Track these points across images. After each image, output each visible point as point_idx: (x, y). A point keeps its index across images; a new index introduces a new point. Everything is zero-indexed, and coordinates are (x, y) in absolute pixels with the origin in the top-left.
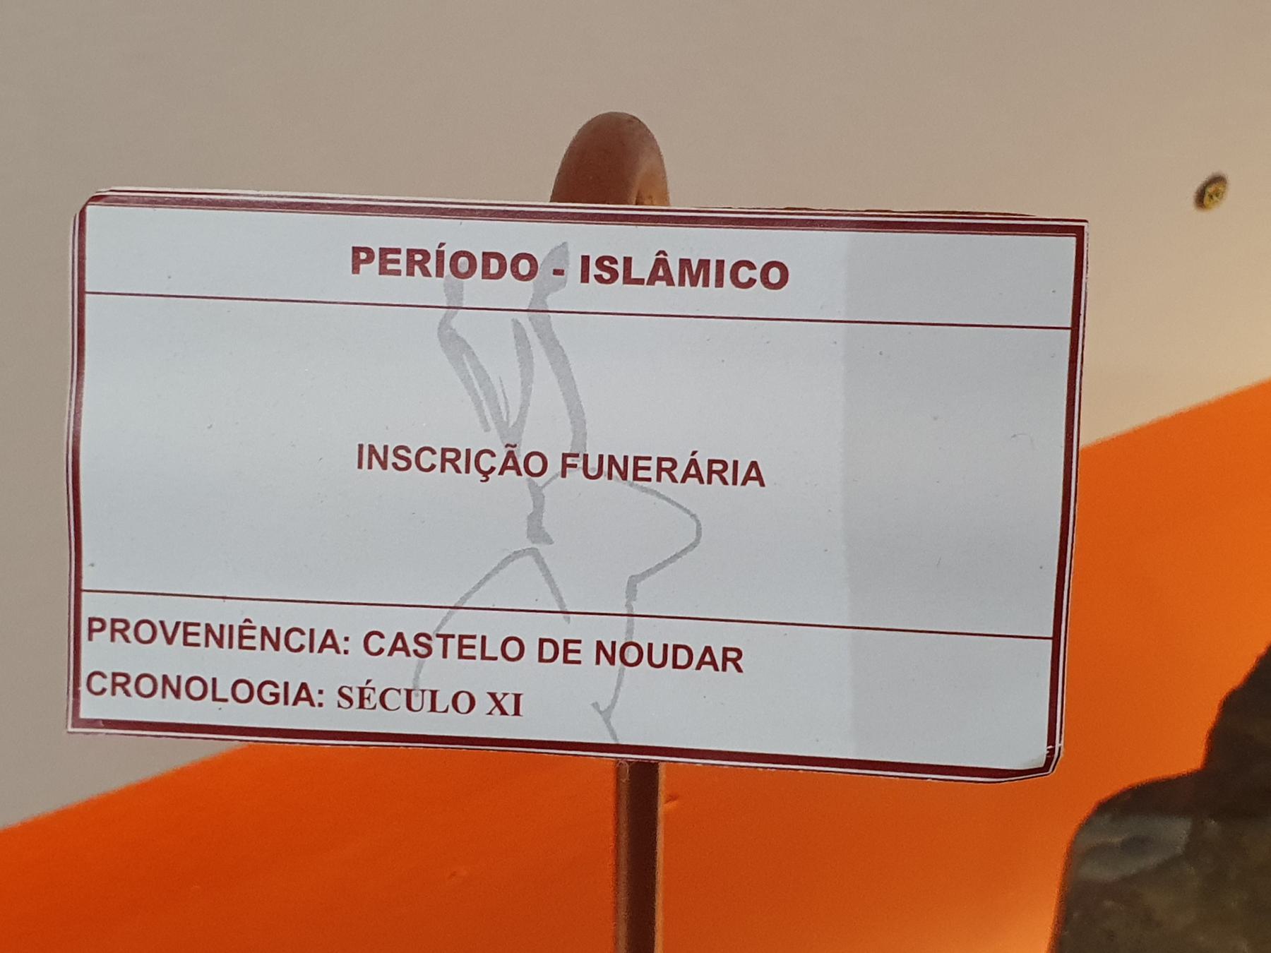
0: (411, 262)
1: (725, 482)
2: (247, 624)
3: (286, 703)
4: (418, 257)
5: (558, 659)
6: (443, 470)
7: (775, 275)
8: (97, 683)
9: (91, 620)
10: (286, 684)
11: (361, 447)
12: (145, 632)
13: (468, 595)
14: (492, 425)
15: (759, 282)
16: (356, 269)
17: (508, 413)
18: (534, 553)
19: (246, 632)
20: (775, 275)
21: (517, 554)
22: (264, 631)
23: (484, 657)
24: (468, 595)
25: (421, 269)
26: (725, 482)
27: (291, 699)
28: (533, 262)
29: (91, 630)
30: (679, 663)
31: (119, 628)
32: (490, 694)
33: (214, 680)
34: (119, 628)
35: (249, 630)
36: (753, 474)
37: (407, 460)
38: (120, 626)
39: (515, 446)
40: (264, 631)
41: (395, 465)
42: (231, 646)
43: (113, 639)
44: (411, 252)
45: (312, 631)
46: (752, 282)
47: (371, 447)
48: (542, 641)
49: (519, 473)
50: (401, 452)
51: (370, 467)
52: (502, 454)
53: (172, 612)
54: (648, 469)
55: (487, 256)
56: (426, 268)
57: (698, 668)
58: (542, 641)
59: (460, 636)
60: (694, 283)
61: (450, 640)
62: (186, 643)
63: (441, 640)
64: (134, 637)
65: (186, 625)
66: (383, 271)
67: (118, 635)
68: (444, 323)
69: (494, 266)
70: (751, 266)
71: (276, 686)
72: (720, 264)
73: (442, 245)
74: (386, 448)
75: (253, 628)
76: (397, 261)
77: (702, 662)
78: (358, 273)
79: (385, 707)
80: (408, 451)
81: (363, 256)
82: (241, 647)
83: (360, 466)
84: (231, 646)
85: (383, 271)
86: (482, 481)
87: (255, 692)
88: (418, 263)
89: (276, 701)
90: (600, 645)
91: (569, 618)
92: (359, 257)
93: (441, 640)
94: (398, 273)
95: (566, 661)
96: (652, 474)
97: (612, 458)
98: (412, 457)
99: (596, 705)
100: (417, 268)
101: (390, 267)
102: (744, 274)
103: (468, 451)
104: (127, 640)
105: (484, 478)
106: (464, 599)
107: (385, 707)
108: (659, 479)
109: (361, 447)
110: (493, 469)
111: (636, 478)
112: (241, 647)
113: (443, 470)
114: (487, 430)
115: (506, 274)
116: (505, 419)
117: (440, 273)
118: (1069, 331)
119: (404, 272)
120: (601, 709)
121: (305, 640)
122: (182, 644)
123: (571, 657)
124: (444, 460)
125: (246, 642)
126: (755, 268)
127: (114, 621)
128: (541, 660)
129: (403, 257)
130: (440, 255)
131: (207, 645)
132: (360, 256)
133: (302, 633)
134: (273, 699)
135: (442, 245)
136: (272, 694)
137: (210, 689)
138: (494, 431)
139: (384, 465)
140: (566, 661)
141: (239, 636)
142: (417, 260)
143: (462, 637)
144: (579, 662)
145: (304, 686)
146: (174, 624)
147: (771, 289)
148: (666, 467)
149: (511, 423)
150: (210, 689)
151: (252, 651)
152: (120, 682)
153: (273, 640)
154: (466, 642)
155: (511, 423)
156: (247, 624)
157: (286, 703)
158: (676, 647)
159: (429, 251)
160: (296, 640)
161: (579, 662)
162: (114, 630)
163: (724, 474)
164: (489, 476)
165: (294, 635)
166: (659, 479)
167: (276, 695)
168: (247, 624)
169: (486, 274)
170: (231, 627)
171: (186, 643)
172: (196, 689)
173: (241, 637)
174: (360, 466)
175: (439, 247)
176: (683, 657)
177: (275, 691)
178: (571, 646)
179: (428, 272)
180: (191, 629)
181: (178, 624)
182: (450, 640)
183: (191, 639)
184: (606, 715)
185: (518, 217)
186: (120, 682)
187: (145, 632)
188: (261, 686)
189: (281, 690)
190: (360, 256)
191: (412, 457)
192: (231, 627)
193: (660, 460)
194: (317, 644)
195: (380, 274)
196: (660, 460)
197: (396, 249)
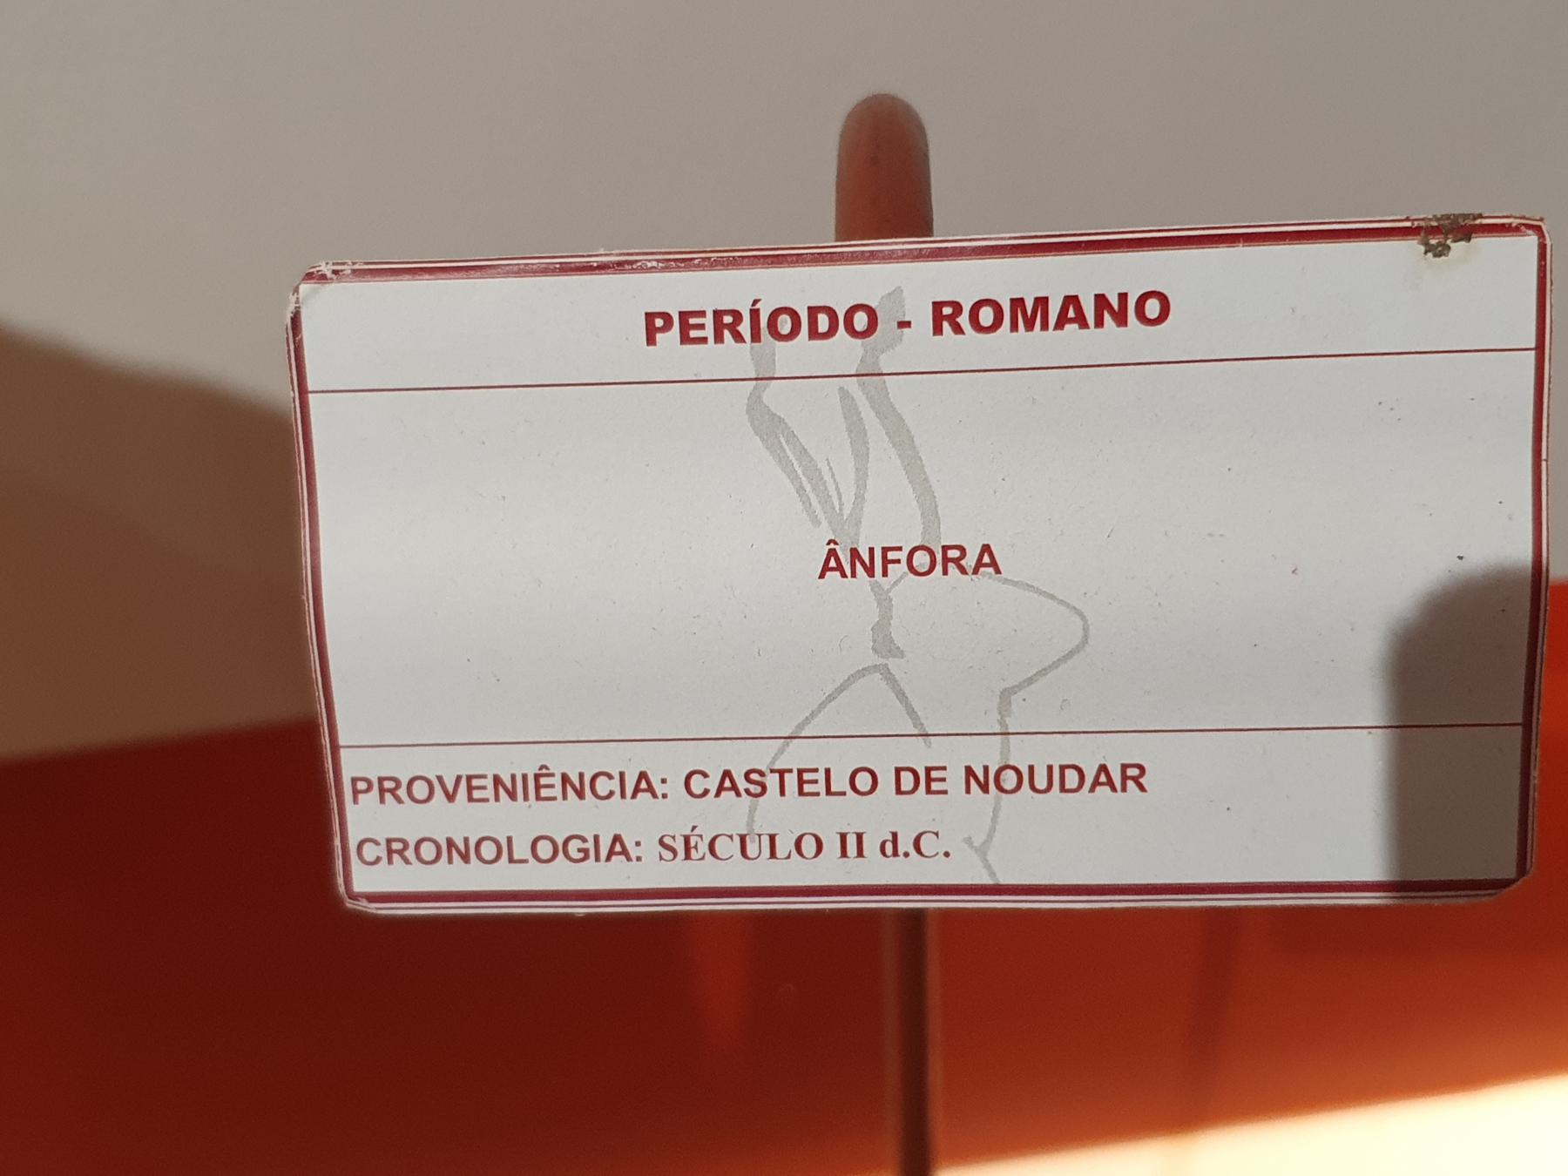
2: (544, 771)
9: (354, 780)
10: (596, 839)
12: (420, 790)
13: (807, 721)
14: (821, 516)
16: (651, 340)
21: (863, 672)
22: (565, 779)
23: (829, 792)
24: (807, 721)
29: (356, 792)
30: (1068, 786)
31: (387, 788)
33: (509, 840)
34: (387, 788)
43: (382, 800)
44: (718, 315)
45: (622, 775)
53: (450, 765)
55: (814, 312)
56: (738, 332)
57: (1092, 790)
58: (898, 771)
60: (1030, 326)
62: (471, 799)
63: (777, 775)
65: (469, 778)
66: (685, 339)
67: (388, 796)
68: (755, 403)
69: (823, 323)
76: (702, 327)
77: (1096, 783)
82: (538, 798)
84: (526, 798)
85: (685, 339)
89: (586, 857)
90: (969, 772)
95: (929, 791)
99: (969, 841)
106: (800, 727)
112: (538, 798)
115: (839, 332)
121: (615, 785)
127: (381, 780)
128: (899, 791)
129: (709, 321)
130: (755, 314)
132: (654, 325)
134: (581, 855)
135: (756, 302)
136: (580, 850)
137: (505, 850)
141: (536, 785)
142: (726, 323)
143: (800, 772)
144: (945, 792)
150: (505, 850)
152: (395, 849)
153: (575, 787)
154: (806, 776)
157: (597, 859)
158: (1063, 768)
161: (945, 792)
162: (382, 791)
169: (814, 334)
170: (525, 777)
172: (488, 850)
173: (538, 787)
176: (1072, 779)
181: (459, 779)
184: (982, 851)
186: (395, 849)
188: (566, 842)
189: (590, 845)
190: (654, 325)
192: (525, 777)
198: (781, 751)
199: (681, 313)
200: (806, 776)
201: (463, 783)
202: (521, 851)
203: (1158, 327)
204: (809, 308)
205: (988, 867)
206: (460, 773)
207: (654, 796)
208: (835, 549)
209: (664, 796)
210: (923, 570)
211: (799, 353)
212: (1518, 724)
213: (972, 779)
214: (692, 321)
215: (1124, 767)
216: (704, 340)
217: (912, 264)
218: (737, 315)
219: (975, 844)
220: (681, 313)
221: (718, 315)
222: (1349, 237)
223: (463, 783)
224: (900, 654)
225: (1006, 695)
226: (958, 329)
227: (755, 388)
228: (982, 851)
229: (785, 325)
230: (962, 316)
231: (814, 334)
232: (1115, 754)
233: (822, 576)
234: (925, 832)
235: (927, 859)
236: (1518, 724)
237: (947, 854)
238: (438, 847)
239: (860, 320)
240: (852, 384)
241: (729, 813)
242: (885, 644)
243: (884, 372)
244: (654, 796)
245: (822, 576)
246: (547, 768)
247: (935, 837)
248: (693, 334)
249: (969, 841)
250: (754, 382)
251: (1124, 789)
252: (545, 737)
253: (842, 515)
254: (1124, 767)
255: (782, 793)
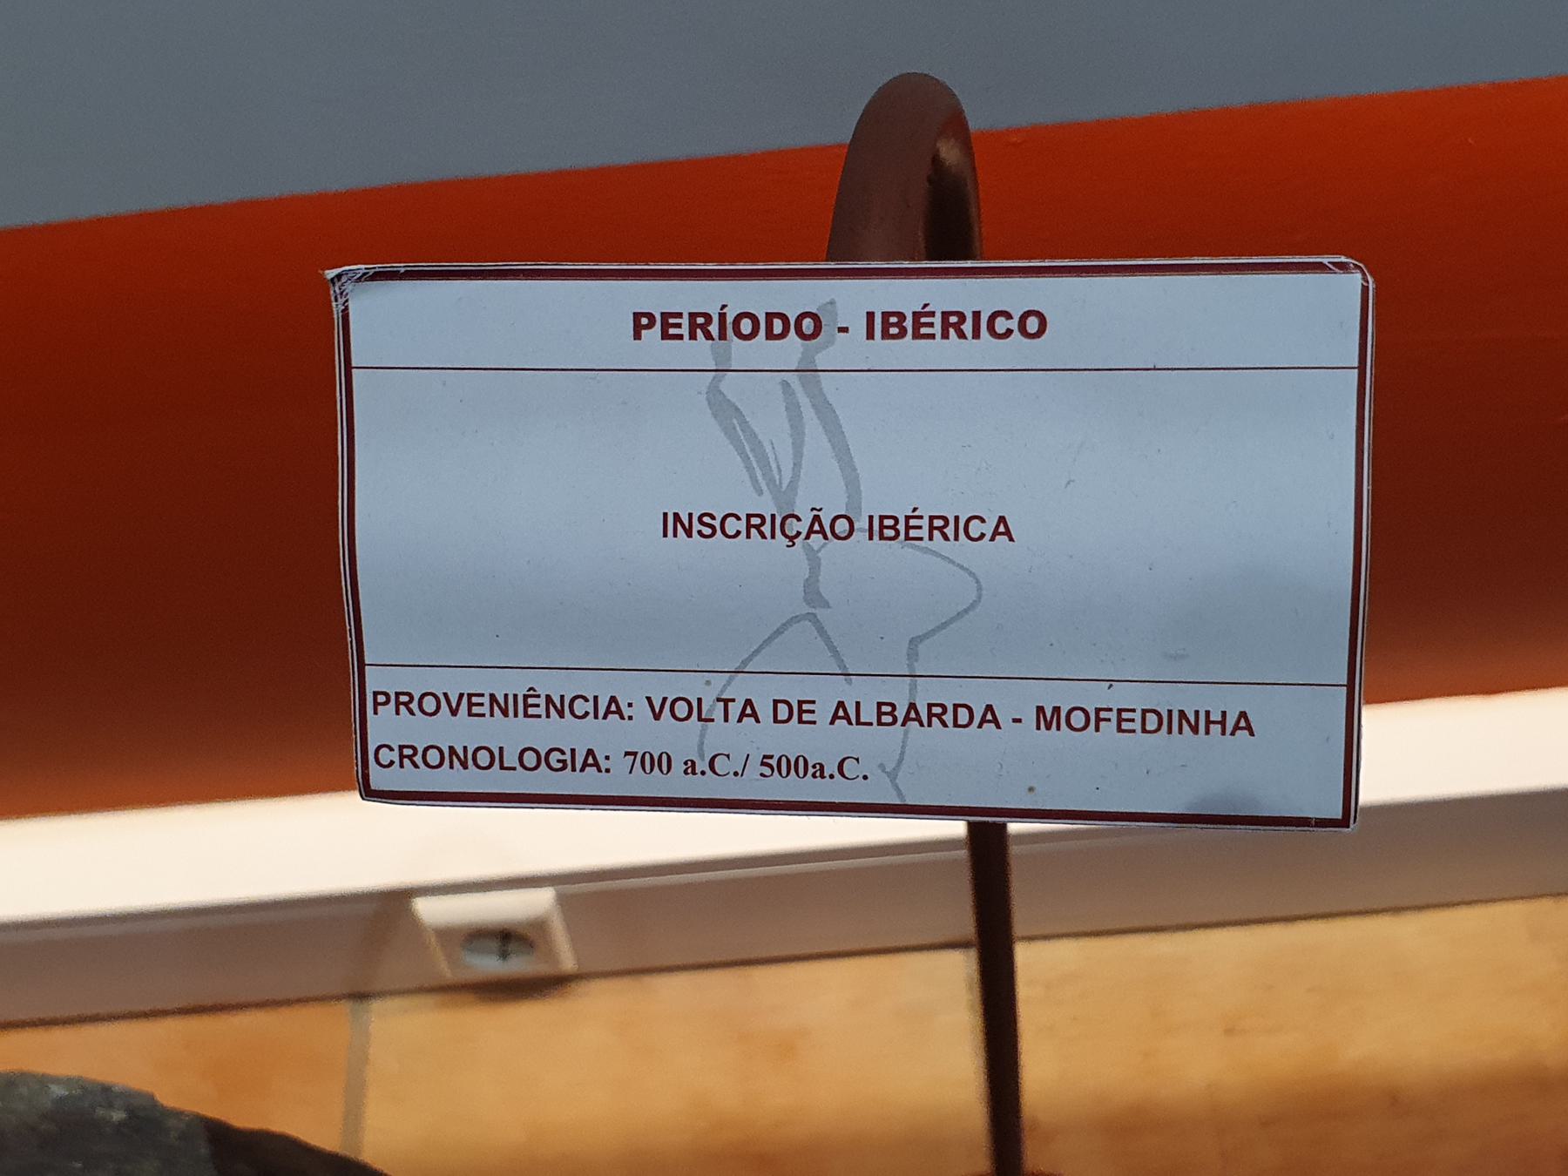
0: (693, 327)
1: (764, 537)
2: (532, 692)
3: (574, 769)
4: (953, 319)
5: (793, 720)
6: (748, 536)
7: (1032, 324)
8: (385, 755)
9: (376, 694)
10: (573, 751)
11: (665, 515)
12: (430, 704)
13: (750, 659)
14: (764, 488)
15: (1016, 333)
16: (637, 336)
17: (781, 476)
18: (812, 618)
19: (531, 701)
20: (1032, 324)
21: (796, 619)
22: (549, 699)
23: (1144, 731)
24: (750, 659)
25: (955, 331)
26: (763, 536)
27: (578, 766)
28: (818, 324)
29: (376, 704)
30: (960, 722)
31: (403, 701)
32: (625, 756)
33: (501, 749)
34: (403, 701)
35: (1126, 713)
36: (1002, 529)
37: (712, 527)
38: (404, 699)
39: (820, 510)
40: (549, 699)
41: (700, 532)
42: (516, 715)
43: (398, 713)
44: (693, 316)
45: (596, 698)
46: (1009, 332)
47: (676, 516)
48: (776, 702)
49: (826, 537)
50: (706, 519)
51: (675, 535)
52: (807, 519)
53: (453, 684)
54: (920, 527)
55: (770, 316)
56: (962, 330)
57: (980, 726)
58: (776, 702)
59: (1118, 709)
61: (730, 704)
62: (470, 714)
63: (722, 704)
64: (418, 710)
65: (470, 696)
66: (665, 336)
67: (402, 708)
68: (714, 390)
69: (778, 326)
70: (1008, 316)
71: (563, 753)
72: (977, 315)
73: (724, 307)
74: (690, 515)
75: (538, 696)
76: (931, 325)
77: (983, 721)
78: (640, 339)
79: (843, 776)
80: (713, 518)
81: (644, 321)
82: (526, 715)
83: (665, 535)
84: (516, 715)
85: (665, 336)
86: (788, 546)
87: (543, 759)
88: (953, 325)
89: (564, 768)
90: (1040, 710)
91: (851, 679)
92: (640, 321)
93: (722, 704)
94: (680, 337)
95: (800, 721)
96: (924, 533)
97: (676, 516)
98: (717, 523)
99: (882, 767)
100: (952, 331)
101: (672, 331)
102: (1001, 325)
103: (957, 518)
104: (412, 713)
105: (791, 544)
106: (745, 663)
107: (843, 776)
108: (931, 538)
109: (665, 515)
110: (799, 533)
111: (907, 538)
112: (526, 715)
113: (748, 536)
114: (760, 492)
115: (790, 334)
116: (778, 482)
117: (976, 335)
118: (1356, 370)
119: (938, 336)
120: (888, 770)
121: (590, 707)
122: (653, 720)
123: (806, 717)
124: (749, 526)
125: (531, 711)
126: (1012, 318)
127: (398, 694)
128: (776, 721)
129: (685, 321)
130: (722, 317)
131: (492, 715)
132: (641, 323)
133: (587, 700)
134: (560, 765)
135: (724, 307)
136: (559, 761)
137: (497, 759)
138: (767, 495)
139: (689, 533)
140: (800, 721)
141: (525, 705)
142: (699, 324)
143: (1120, 711)
144: (814, 723)
145: (590, 752)
146: (457, 696)
147: (996, 338)
148: (939, 525)
149: (784, 486)
151: (812, 725)
153: (558, 707)
154: (1125, 715)
155: (784, 486)
156: (531, 693)
157: (574, 769)
158: (956, 706)
159: (654, 313)
160: (580, 708)
161: (814, 723)
162: (398, 704)
163: (762, 528)
164: (795, 541)
165: (578, 702)
166: (931, 538)
167: (564, 762)
168: (532, 692)
169: (770, 335)
170: (515, 696)
171: (470, 714)
172: (483, 758)
173: (526, 706)
174: (665, 535)
175: (721, 309)
176: (963, 716)
177: (562, 757)
178: (805, 707)
179: (712, 336)
180: (475, 700)
181: (461, 696)
182: (730, 704)
183: (475, 710)
184: (893, 776)
185: (1278, 270)
186: (407, 755)
187: (430, 704)
188: (548, 754)
189: (568, 757)
190: (641, 323)
191: (717, 523)
192: (515, 696)
193: (932, 518)
194: (602, 712)
195: (662, 339)
196: (932, 518)
197: (677, 313)
198: (729, 682)
199: (663, 314)
200: (1125, 715)
201: (465, 699)
202: (511, 759)
203: (782, 341)
204: (767, 314)
205: (897, 788)
206: (462, 692)
207: (622, 718)
208: (818, 516)
209: (630, 718)
210: (843, 535)
211: (760, 351)
212: (1344, 685)
213: (1184, 722)
214: (671, 321)
215: (930, 706)
216: (680, 337)
217: (918, 280)
218: (708, 317)
219: (888, 770)
220: (663, 314)
221: (945, 315)
222: (1314, 269)
223: (465, 699)
224: (827, 605)
225: (914, 642)
226: (962, 335)
227: (714, 378)
228: (893, 776)
229: (746, 326)
230: (966, 324)
231: (770, 335)
232: (1231, 702)
233: (832, 723)
234: (848, 758)
235: (721, 778)
236: (1344, 685)
237: (865, 777)
238: (474, 759)
239: (808, 325)
240: (793, 379)
241: (678, 739)
242: (813, 594)
243: (819, 369)
244: (622, 718)
245: (832, 723)
246: (535, 691)
247: (855, 762)
248: (924, 330)
249: (882, 767)
250: (714, 373)
251: (930, 725)
252: (1133, 677)
253: (781, 487)
254: (930, 706)
255: (726, 720)
